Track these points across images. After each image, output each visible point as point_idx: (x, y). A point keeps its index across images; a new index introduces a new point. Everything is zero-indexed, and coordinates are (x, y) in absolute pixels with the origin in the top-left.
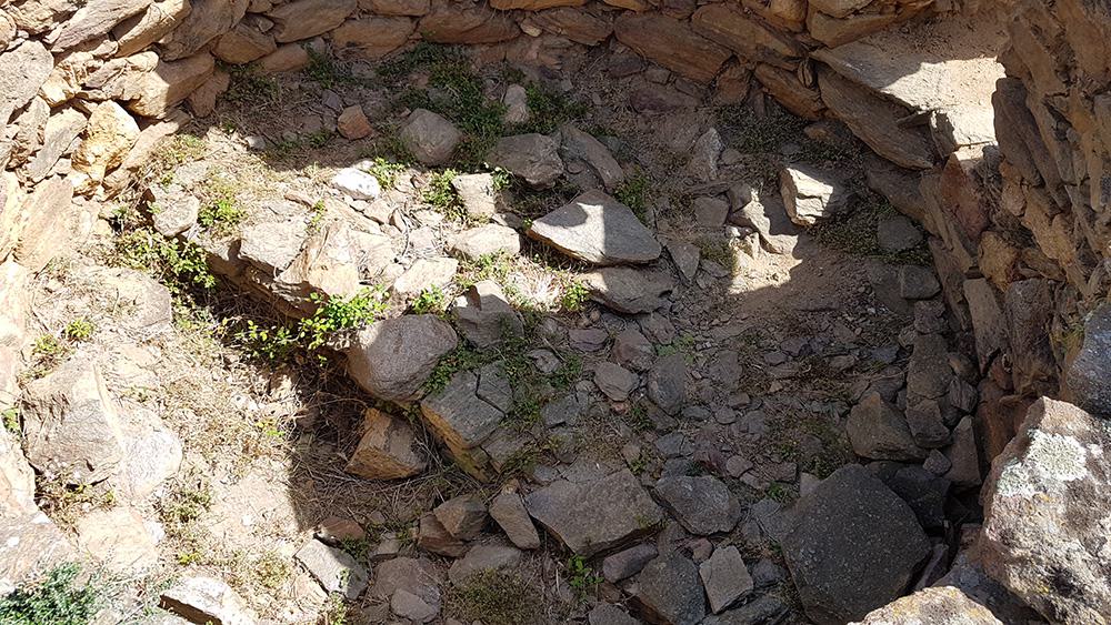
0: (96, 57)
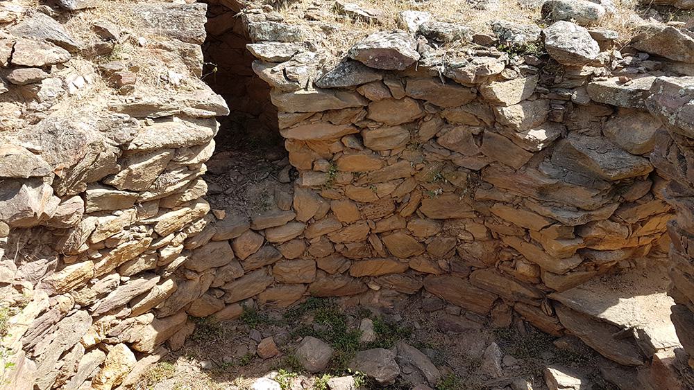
0: (117, 318)
